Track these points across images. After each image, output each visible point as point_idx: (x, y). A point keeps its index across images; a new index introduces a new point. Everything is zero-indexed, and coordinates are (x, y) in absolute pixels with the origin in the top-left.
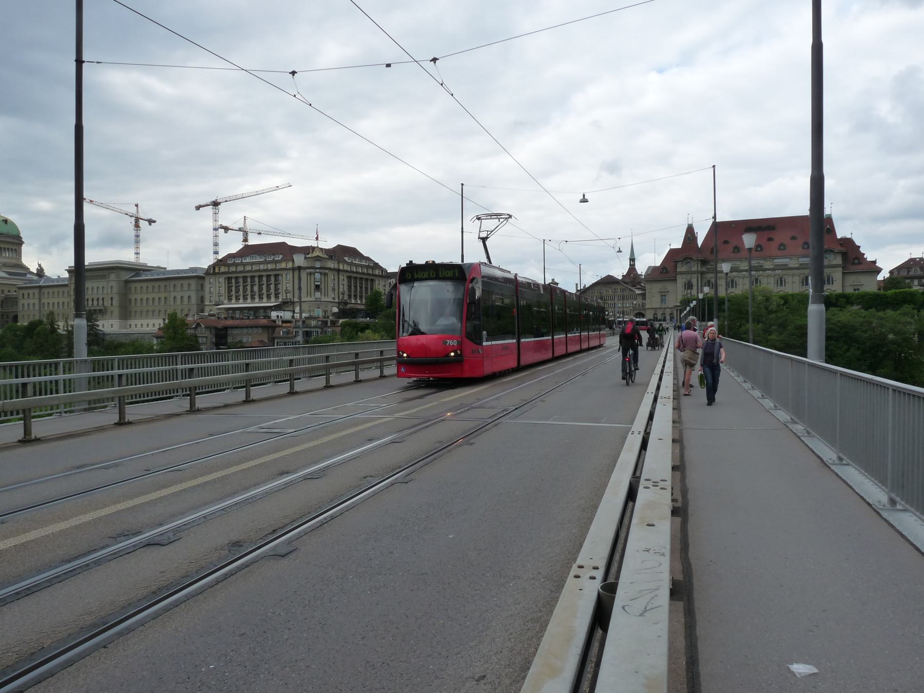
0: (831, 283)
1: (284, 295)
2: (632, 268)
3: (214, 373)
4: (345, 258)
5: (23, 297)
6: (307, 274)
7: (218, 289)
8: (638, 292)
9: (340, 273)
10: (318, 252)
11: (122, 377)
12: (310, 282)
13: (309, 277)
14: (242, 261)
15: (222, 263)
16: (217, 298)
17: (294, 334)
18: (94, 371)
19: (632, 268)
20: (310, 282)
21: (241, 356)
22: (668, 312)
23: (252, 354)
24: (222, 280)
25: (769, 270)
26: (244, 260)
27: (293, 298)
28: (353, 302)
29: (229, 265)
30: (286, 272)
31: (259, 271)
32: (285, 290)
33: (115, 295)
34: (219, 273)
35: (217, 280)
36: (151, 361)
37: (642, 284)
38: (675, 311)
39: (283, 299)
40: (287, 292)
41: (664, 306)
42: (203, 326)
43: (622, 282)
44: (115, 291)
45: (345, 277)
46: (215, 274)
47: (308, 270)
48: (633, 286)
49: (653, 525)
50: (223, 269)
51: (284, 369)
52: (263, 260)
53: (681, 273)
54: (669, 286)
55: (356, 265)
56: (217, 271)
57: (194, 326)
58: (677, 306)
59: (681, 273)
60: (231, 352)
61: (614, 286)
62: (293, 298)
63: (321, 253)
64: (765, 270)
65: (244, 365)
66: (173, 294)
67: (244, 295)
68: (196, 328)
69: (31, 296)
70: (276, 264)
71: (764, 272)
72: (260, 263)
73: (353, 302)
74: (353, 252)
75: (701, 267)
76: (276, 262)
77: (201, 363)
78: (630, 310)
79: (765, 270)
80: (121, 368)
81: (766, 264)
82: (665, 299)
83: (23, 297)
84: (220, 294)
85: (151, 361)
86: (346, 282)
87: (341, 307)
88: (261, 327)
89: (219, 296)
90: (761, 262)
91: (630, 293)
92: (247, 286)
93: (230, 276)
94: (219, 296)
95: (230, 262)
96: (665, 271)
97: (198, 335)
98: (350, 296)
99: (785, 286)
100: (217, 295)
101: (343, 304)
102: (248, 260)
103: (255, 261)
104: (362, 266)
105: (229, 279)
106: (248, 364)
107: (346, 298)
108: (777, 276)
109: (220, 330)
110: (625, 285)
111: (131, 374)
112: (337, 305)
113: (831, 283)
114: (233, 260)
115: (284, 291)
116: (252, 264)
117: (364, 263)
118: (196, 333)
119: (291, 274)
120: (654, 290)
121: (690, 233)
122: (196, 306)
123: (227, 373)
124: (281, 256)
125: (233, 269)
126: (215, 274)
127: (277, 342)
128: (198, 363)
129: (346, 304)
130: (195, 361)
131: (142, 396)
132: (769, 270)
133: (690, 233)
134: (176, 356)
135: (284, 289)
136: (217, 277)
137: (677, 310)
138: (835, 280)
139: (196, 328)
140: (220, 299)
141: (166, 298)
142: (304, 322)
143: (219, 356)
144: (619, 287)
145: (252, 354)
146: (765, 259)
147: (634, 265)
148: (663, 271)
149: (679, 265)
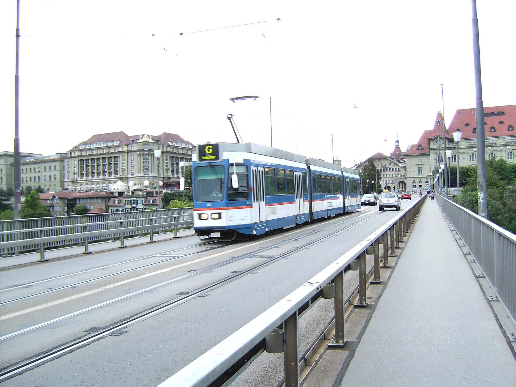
0: (513, 157)
1: (121, 172)
2: (398, 148)
3: (32, 236)
4: (168, 142)
5: (50, 170)
6: (138, 155)
7: (73, 168)
8: (401, 165)
9: (164, 153)
10: (146, 138)
11: (122, 224)
12: (140, 162)
13: (139, 157)
14: (90, 147)
15: (76, 149)
16: (73, 175)
17: (124, 203)
18: (41, 227)
19: (398, 148)
20: (140, 162)
21: (93, 219)
22: (424, 180)
23: (100, 218)
24: (77, 162)
25: (501, 146)
26: (92, 146)
27: (128, 174)
28: (176, 176)
29: (81, 151)
30: (122, 154)
31: (108, 153)
32: (122, 169)
33: (4, 175)
34: (74, 157)
35: (73, 161)
36: (34, 223)
37: (404, 159)
38: (430, 179)
39: (120, 176)
40: (123, 170)
41: (421, 176)
42: (57, 198)
43: (389, 158)
44: (4, 172)
45: (169, 157)
46: (71, 158)
47: (139, 152)
48: (397, 161)
49: (219, 354)
50: (77, 154)
51: (137, 227)
52: (106, 146)
53: (434, 149)
54: (424, 160)
55: (178, 148)
56: (73, 155)
57: (51, 198)
58: (430, 176)
59: (434, 149)
60: (40, 220)
61: (383, 162)
62: (128, 174)
63: (149, 139)
64: (498, 146)
65: (149, 220)
66: (44, 174)
67: (103, 172)
68: (52, 199)
69: (53, 168)
70: (81, 152)
71: (497, 148)
72: (103, 148)
73: (176, 176)
74: (176, 138)
75: (449, 144)
76: (115, 147)
77: (49, 226)
78: (395, 179)
79: (498, 146)
80: (43, 226)
81: (499, 141)
82: (421, 170)
83: (50, 170)
84: (75, 173)
85: (34, 223)
86: (169, 162)
87: (166, 181)
88: (101, 198)
89: (74, 174)
90: (495, 140)
91: (395, 166)
92: (83, 167)
93: (82, 159)
94: (74, 174)
95: (82, 148)
96: (420, 148)
97: (54, 205)
98: (172, 172)
99: (514, 158)
100: (73, 173)
101: (166, 178)
102: (95, 146)
103: (99, 146)
104: (183, 149)
105: (81, 161)
106: (86, 226)
107: (169, 173)
108: (507, 151)
109: (70, 200)
110: (392, 160)
111: (35, 232)
112: (162, 179)
113: (513, 157)
114: (84, 146)
115: (121, 169)
116: (98, 149)
117: (184, 146)
118: (53, 203)
119: (126, 156)
120: (412, 164)
121: (440, 119)
122: (59, 182)
123: (107, 229)
124: (119, 142)
125: (84, 153)
126: (71, 157)
127: (111, 210)
128: (105, 221)
129: (169, 178)
130: (52, 224)
131: (28, 248)
132: (502, 146)
133: (440, 119)
134: (37, 220)
135: (121, 167)
136: (73, 159)
137: (431, 178)
138: (497, 157)
139: (52, 199)
140: (75, 176)
141: (39, 177)
142: (133, 193)
143: (103, 217)
144: (386, 162)
145: (100, 218)
146: (497, 137)
147: (398, 145)
148: (419, 148)
149: (431, 143)
